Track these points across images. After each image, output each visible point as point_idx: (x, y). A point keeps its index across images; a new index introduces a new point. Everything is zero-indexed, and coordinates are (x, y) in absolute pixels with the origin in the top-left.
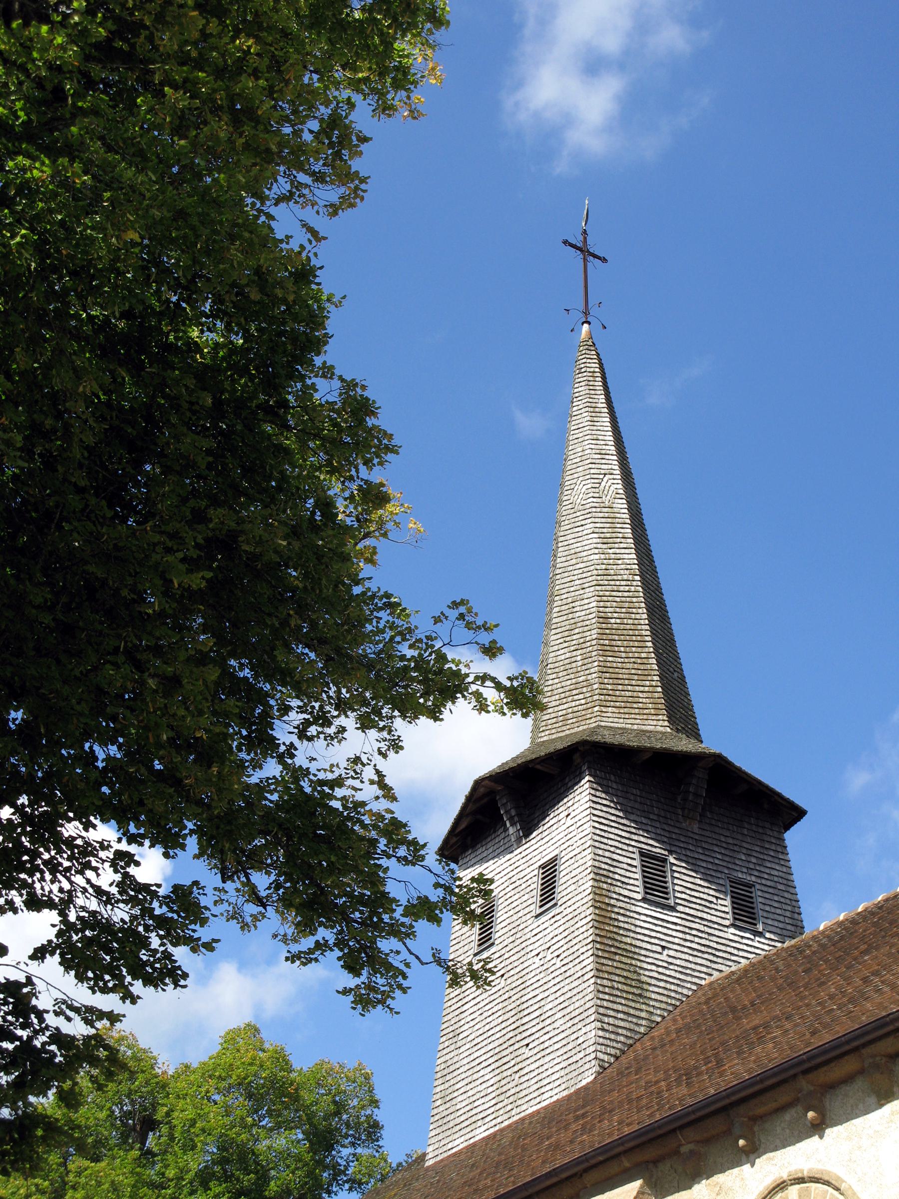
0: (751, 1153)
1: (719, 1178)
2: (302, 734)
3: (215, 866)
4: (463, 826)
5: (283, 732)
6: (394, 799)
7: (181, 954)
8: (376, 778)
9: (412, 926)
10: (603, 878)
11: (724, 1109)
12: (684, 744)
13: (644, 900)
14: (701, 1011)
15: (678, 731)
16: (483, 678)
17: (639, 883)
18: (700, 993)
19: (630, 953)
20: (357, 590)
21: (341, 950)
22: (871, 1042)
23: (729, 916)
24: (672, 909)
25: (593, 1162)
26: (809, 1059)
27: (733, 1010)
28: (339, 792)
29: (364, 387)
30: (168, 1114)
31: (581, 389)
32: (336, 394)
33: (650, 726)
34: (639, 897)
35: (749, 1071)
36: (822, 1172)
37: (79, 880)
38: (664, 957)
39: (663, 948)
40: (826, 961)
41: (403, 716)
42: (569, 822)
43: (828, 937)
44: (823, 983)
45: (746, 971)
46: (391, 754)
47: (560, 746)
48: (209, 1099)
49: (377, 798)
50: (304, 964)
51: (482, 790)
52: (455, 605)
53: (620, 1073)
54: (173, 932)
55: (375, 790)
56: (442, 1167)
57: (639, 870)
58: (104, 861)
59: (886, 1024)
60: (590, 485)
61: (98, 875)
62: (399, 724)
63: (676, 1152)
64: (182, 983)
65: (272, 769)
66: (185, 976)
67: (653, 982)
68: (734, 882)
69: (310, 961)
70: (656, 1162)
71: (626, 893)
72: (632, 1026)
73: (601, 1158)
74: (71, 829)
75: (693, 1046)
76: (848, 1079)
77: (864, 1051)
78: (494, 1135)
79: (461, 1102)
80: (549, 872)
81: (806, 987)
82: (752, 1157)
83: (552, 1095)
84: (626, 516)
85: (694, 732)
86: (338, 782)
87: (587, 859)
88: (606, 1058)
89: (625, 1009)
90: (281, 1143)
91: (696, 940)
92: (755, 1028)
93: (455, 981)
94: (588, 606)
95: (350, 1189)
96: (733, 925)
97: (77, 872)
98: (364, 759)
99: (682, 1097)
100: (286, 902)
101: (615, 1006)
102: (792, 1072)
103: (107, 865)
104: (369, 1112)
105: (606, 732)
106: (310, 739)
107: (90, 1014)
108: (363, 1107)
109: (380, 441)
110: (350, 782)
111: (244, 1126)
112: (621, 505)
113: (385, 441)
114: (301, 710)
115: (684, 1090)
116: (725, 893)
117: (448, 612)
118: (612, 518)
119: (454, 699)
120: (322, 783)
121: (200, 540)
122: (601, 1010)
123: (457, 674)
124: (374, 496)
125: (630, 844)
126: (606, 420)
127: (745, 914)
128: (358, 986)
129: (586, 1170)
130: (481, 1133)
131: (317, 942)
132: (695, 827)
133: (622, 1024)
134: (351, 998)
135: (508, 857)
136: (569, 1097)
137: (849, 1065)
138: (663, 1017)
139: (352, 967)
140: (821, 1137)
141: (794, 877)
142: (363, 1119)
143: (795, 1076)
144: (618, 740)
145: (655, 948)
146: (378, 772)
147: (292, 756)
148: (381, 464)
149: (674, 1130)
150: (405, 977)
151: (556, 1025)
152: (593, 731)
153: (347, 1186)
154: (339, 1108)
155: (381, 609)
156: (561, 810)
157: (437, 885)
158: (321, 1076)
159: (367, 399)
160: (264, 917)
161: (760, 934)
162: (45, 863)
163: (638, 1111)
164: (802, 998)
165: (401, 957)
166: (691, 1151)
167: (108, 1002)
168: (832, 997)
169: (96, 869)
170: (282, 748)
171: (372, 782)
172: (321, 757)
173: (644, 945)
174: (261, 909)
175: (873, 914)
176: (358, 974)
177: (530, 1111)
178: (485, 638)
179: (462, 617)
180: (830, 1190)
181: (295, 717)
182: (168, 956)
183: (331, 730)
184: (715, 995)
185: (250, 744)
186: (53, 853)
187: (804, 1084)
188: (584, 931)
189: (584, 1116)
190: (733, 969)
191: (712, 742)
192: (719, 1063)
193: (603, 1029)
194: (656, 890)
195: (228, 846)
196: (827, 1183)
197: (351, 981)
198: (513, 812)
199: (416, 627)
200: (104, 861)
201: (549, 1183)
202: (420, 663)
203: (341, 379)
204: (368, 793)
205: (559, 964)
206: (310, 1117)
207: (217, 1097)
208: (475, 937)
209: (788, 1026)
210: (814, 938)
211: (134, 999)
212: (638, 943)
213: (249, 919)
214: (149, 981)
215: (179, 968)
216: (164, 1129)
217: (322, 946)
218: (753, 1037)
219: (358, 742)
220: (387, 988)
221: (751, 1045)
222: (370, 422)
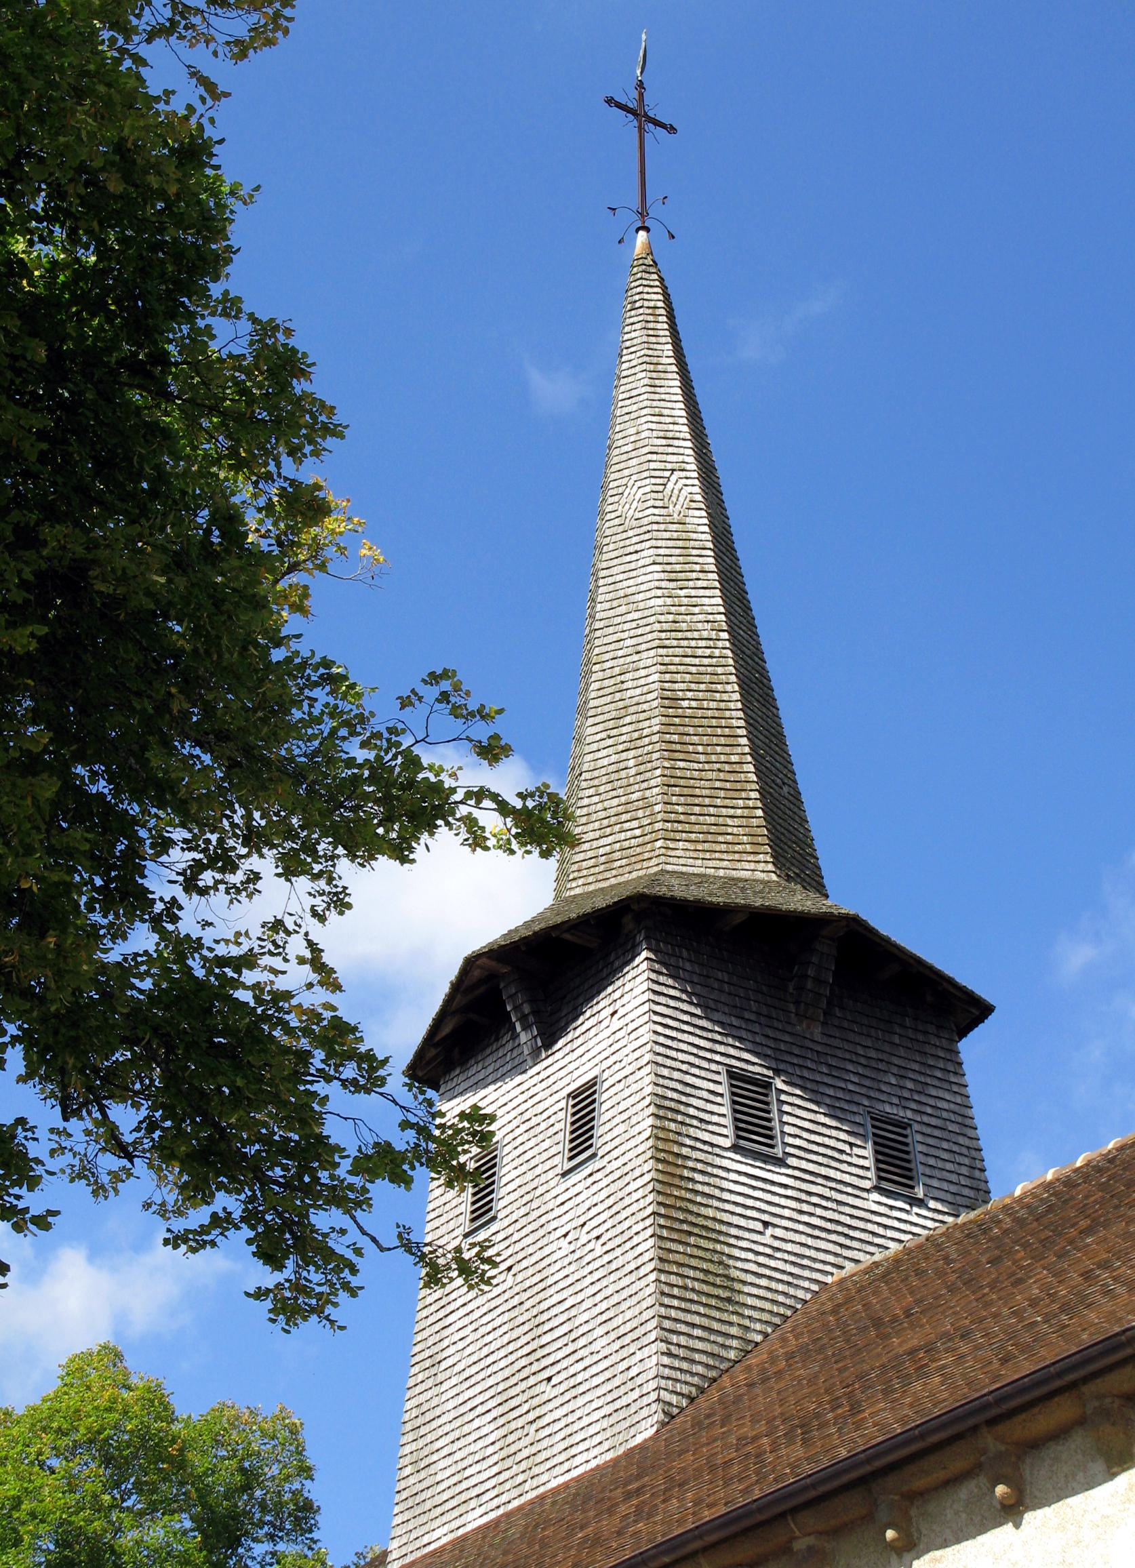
2: (191, 884)
3: (52, 1095)
4: (446, 1030)
5: (160, 881)
6: (337, 987)
10: (668, 1112)
11: (863, 1481)
12: (799, 900)
13: (735, 1148)
14: (825, 1325)
15: (789, 878)
16: (479, 795)
18: (824, 1297)
19: (713, 1232)
20: (277, 655)
21: (253, 1228)
24: (781, 1162)
26: (998, 1402)
27: (877, 1323)
28: (249, 977)
29: (289, 332)
31: (635, 334)
32: (244, 342)
33: (738, 868)
34: (727, 1143)
35: (903, 1420)
38: (767, 1239)
39: (766, 1224)
40: (1025, 1246)
41: (352, 856)
42: (616, 1024)
43: (1028, 1206)
44: (1020, 1281)
45: (897, 1261)
46: (332, 916)
47: (601, 903)
49: (310, 986)
50: (194, 1250)
51: (476, 973)
52: (434, 678)
53: (697, 1424)
55: (306, 973)
57: (726, 1100)
60: (648, 488)
62: (345, 868)
63: (786, 1550)
65: (142, 939)
67: (750, 1278)
68: (880, 1121)
69: (203, 1245)
72: (716, 1350)
76: (1060, 1434)
77: (1088, 1389)
78: (496, 1522)
79: (443, 1469)
80: (584, 1104)
81: (993, 1286)
83: (589, 1459)
85: (815, 883)
86: (248, 961)
87: (645, 1082)
88: (674, 1399)
89: (705, 1322)
91: (819, 1212)
92: (912, 1352)
96: (877, 1188)
98: (289, 923)
100: (165, 1152)
101: (689, 1318)
102: (971, 1422)
104: (296, 1486)
105: (674, 881)
106: (203, 892)
108: (287, 1478)
110: (266, 960)
111: (98, 1508)
112: (699, 520)
113: (323, 418)
114: (189, 845)
115: (798, 1451)
116: (864, 1137)
117: (423, 690)
118: (684, 541)
119: (432, 829)
120: (222, 961)
121: (28, 575)
122: (667, 1324)
123: (436, 789)
125: (713, 1061)
126: (673, 384)
127: (896, 1171)
128: (279, 1286)
130: (475, 1519)
131: (214, 1215)
132: (817, 1032)
133: (699, 1345)
134: (268, 1304)
136: (615, 1462)
137: (1062, 1411)
138: (766, 1335)
139: (270, 1255)
140: (1017, 1526)
141: (974, 1112)
143: (975, 1429)
144: (693, 893)
146: (311, 945)
147: (175, 919)
148: (316, 453)
149: (782, 1515)
150: (354, 1271)
151: (595, 1347)
152: (654, 879)
154: (250, 1479)
156: (603, 1004)
157: (405, 1125)
159: (294, 351)
160: (130, 1175)
161: (921, 1203)
164: (987, 1305)
165: (347, 1239)
166: (810, 1548)
168: (1034, 1303)
170: (159, 907)
171: (302, 961)
172: (221, 920)
174: (125, 1162)
175: (1099, 1170)
176: (279, 1267)
177: (554, 1484)
178: (481, 731)
179: (444, 697)
181: (180, 858)
183: (237, 878)
184: (848, 1300)
187: (990, 1442)
188: (640, 1197)
189: (639, 1491)
190: (877, 1257)
192: (855, 1408)
193: (669, 1354)
194: (754, 1132)
195: (71, 1056)
197: (269, 1278)
198: (527, 1009)
202: (378, 770)
203: (253, 318)
204: (295, 977)
205: (566, 1249)
206: (204, 1494)
207: (55, 1463)
209: (964, 1348)
213: (105, 1179)
217: (221, 1222)
219: (280, 895)
221: (906, 1380)
222: (299, 386)
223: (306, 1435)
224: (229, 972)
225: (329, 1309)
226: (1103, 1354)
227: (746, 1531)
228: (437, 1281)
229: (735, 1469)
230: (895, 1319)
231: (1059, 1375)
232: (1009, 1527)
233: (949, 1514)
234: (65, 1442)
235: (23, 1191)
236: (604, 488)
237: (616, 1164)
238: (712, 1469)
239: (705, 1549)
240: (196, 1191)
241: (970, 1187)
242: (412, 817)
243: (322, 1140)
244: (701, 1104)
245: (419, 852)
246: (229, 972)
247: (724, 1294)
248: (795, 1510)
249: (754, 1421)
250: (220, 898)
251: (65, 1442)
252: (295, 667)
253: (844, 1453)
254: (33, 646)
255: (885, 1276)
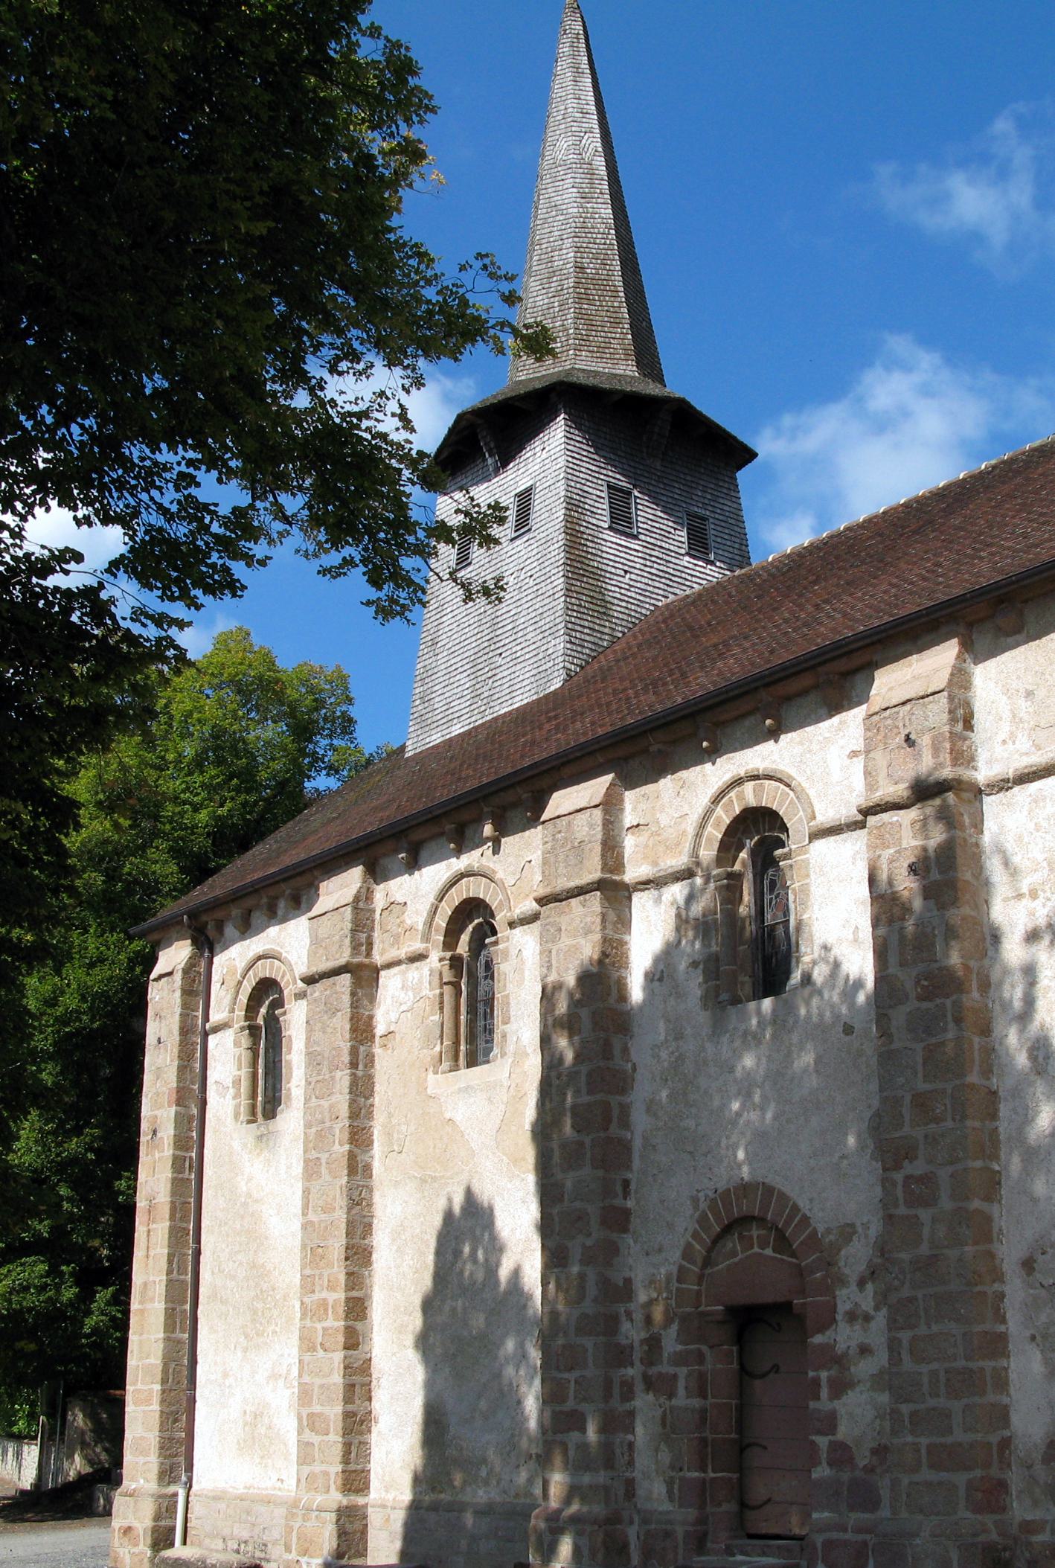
0: (713, 754)
1: (683, 774)
2: (333, 370)
3: (246, 487)
4: (443, 457)
5: (314, 367)
6: (413, 430)
7: (238, 568)
8: (399, 411)
9: (435, 547)
10: (574, 507)
12: (652, 389)
13: (610, 528)
14: (659, 629)
15: (645, 375)
16: (503, 324)
17: (607, 513)
18: (657, 613)
19: (597, 575)
20: (392, 237)
21: (366, 566)
22: (825, 662)
23: (685, 546)
24: (635, 537)
25: (572, 757)
26: (771, 674)
27: (691, 628)
28: (365, 424)
29: (407, 49)
30: (166, 706)
31: (565, 49)
32: (380, 53)
33: (618, 368)
34: (606, 526)
35: (714, 683)
36: (775, 771)
37: (144, 496)
38: (626, 580)
39: (626, 572)
40: (777, 589)
41: (426, 355)
42: (545, 455)
43: (777, 567)
44: (777, 609)
45: (700, 595)
46: (413, 390)
47: (538, 385)
48: (201, 692)
49: (397, 429)
50: (334, 578)
51: (464, 423)
52: (480, 256)
53: (586, 681)
54: (227, 546)
55: (396, 422)
56: (421, 758)
57: (606, 501)
58: (167, 481)
59: (841, 647)
60: (571, 138)
61: (162, 494)
64: (239, 593)
65: (301, 400)
66: (244, 588)
67: (616, 602)
68: (691, 516)
69: (339, 575)
70: (626, 759)
71: (594, 521)
72: (597, 641)
73: (578, 754)
74: (136, 451)
75: (654, 659)
76: (803, 693)
77: (820, 669)
78: (469, 732)
79: (438, 703)
80: (525, 498)
81: (760, 610)
82: (713, 757)
84: (603, 171)
85: (659, 378)
86: (364, 415)
88: (573, 667)
89: (591, 625)
90: (267, 733)
91: (656, 565)
92: (715, 646)
93: (468, 598)
94: (566, 257)
95: (328, 775)
96: (687, 554)
97: (143, 490)
98: (389, 393)
99: (650, 704)
100: (316, 521)
101: (582, 623)
102: (753, 686)
103: (171, 485)
104: (344, 708)
105: (581, 375)
106: (340, 374)
107: (160, 620)
108: (338, 704)
109: (421, 100)
110: (376, 415)
111: (236, 718)
112: (600, 163)
113: (426, 101)
116: (682, 525)
118: (591, 174)
119: (474, 341)
120: (350, 414)
121: (265, 188)
122: (570, 626)
123: (477, 319)
124: (414, 153)
125: (599, 479)
126: (588, 81)
127: (699, 545)
128: (379, 599)
129: (563, 764)
130: (457, 730)
131: (344, 559)
132: (658, 465)
133: (588, 638)
134: (374, 608)
135: (486, 485)
136: (539, 700)
137: (806, 680)
138: (624, 633)
139: (375, 582)
140: (776, 741)
141: (743, 513)
142: (338, 714)
143: (756, 689)
144: (591, 381)
145: (618, 572)
146: (401, 406)
147: (322, 389)
148: (421, 122)
149: (645, 732)
150: (424, 592)
151: (528, 637)
152: (569, 373)
153: (324, 772)
154: (319, 704)
155: (411, 257)
156: (537, 444)
157: (457, 511)
158: (306, 678)
159: (411, 59)
160: (288, 533)
161: (712, 563)
162: (113, 481)
163: (610, 714)
164: (758, 621)
165: (422, 574)
166: (659, 751)
167: (177, 610)
168: (786, 621)
169: (160, 489)
170: (314, 381)
171: (393, 415)
172: (346, 391)
173: (609, 569)
174: (288, 527)
175: (817, 548)
176: (380, 588)
177: (503, 712)
178: (505, 287)
179: (485, 267)
180: (782, 786)
182: (226, 570)
183: (360, 367)
184: (672, 616)
185: (283, 376)
186: (120, 472)
188: (556, 553)
189: (556, 717)
190: (688, 592)
191: (677, 384)
193: (570, 642)
194: (621, 520)
195: (263, 470)
196: (780, 780)
197: (372, 593)
198: (492, 445)
199: (443, 274)
200: (167, 481)
201: (530, 773)
202: (443, 307)
203: (387, 39)
204: (389, 425)
205: (531, 583)
206: (293, 708)
207: (209, 692)
208: (454, 557)
209: (746, 644)
210: (763, 568)
211: (198, 607)
212: (604, 567)
213: (275, 536)
214: (209, 590)
215: (238, 581)
216: (163, 719)
217: (348, 562)
218: (714, 654)
219: (385, 377)
220: (407, 602)
221: (714, 661)
222: (412, 81)
223: (350, 680)
224: (355, 421)
225: (407, 613)
226: (832, 650)
227: (623, 741)
228: (472, 600)
229: (614, 707)
230: (701, 627)
231: (806, 661)
232: (772, 742)
233: (738, 734)
234: (216, 681)
235: (251, 545)
236: (544, 140)
237: (542, 535)
238: (600, 706)
239: (600, 749)
240: (336, 543)
241: (739, 556)
242: (463, 335)
243: (407, 518)
244: (592, 503)
245: (465, 357)
246: (355, 421)
247: (602, 610)
248: (652, 730)
249: (622, 679)
250: (350, 378)
251: (216, 681)
252: (400, 246)
253: (680, 700)
254: (265, 232)
255: (693, 603)
